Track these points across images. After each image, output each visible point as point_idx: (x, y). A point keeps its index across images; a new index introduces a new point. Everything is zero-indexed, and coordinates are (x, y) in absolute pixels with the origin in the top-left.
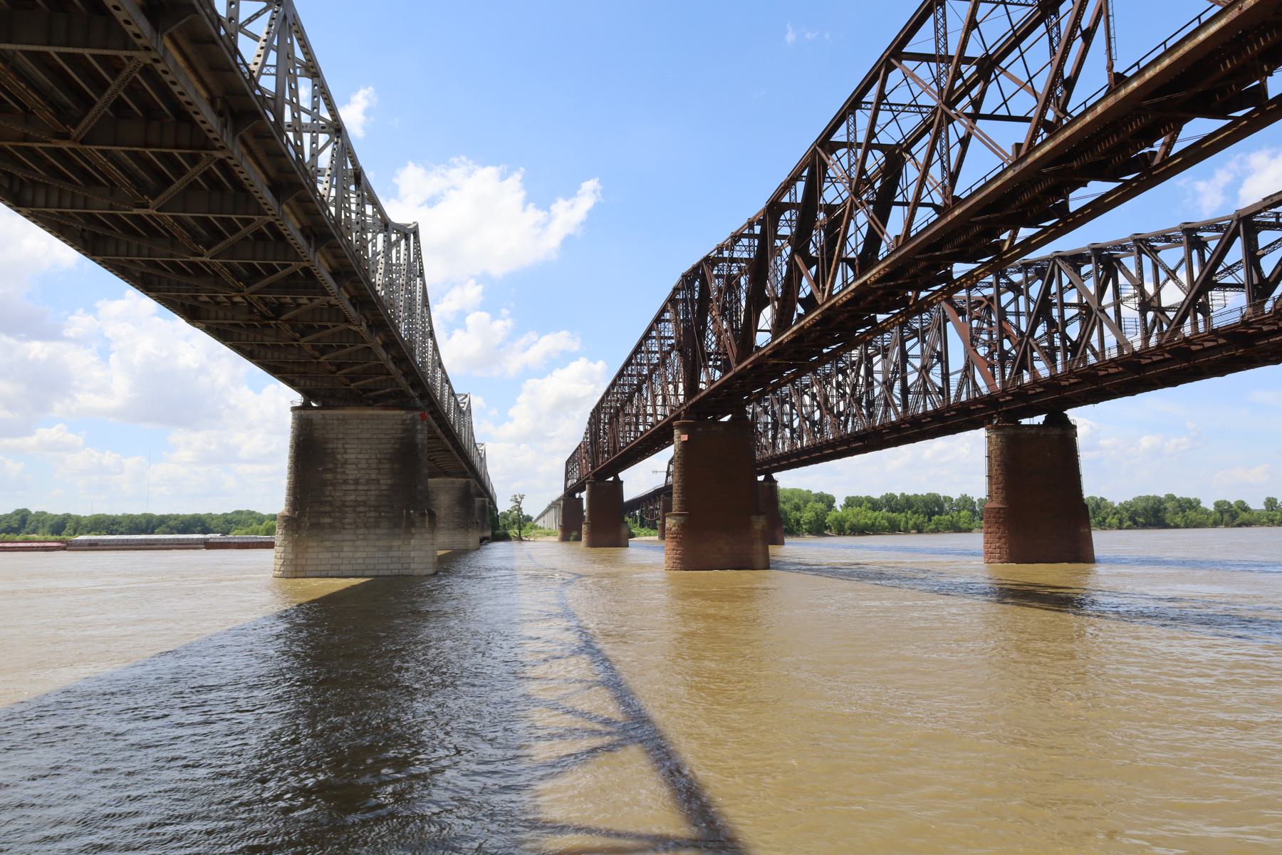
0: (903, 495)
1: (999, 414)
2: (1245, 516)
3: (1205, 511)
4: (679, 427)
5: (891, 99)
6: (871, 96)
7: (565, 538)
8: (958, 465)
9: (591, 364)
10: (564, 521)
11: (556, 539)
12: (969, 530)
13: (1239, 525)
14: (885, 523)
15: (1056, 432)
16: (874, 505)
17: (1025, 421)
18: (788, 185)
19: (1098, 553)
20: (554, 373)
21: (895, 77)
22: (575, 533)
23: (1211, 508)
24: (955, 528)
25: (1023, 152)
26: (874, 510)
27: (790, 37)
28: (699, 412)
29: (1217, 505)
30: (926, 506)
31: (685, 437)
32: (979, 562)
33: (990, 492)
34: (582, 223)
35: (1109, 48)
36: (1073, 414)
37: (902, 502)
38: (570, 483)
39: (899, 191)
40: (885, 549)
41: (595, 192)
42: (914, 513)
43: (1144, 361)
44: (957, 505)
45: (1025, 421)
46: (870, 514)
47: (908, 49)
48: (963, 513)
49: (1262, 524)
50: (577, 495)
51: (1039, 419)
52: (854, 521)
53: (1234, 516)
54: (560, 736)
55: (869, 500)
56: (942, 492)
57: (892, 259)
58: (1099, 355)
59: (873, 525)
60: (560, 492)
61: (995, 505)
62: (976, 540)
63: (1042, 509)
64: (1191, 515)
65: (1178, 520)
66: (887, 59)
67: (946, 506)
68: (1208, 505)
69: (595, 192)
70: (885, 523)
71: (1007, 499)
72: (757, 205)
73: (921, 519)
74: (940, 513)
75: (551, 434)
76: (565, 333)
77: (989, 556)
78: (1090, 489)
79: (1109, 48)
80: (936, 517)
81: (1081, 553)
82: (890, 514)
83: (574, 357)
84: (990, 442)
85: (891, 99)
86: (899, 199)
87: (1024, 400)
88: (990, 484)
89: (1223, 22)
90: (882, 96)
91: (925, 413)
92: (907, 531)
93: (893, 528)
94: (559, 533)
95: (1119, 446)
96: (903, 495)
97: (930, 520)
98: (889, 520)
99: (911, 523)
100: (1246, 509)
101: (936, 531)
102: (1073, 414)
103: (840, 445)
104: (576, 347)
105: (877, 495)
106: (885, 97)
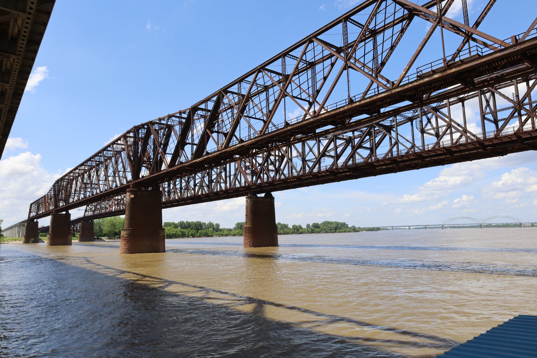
0: (187, 222)
1: (250, 192)
2: (301, 230)
3: (290, 229)
4: (129, 191)
5: (257, 82)
6: (251, 79)
7: (27, 241)
8: (233, 211)
9: (33, 156)
10: (26, 233)
11: (22, 242)
12: (212, 236)
13: (299, 234)
14: (180, 233)
15: (269, 200)
16: (176, 226)
17: (259, 195)
18: (206, 101)
19: (279, 243)
20: (10, 158)
21: (260, 75)
22: (33, 239)
23: (291, 227)
24: (207, 235)
25: (316, 114)
26: (176, 228)
27: (148, 26)
28: (137, 186)
29: (293, 226)
30: (196, 226)
31: (132, 196)
32: (242, 247)
33: (246, 221)
34: (35, 87)
35: (349, 91)
36: (274, 194)
37: (187, 225)
38: (87, 213)
39: (245, 111)
40: (176, 243)
41: (45, 73)
42: (192, 229)
43: (303, 178)
44: (208, 226)
45: (259, 195)
46: (174, 229)
47: (266, 67)
48: (210, 229)
49: (306, 233)
50: (35, 220)
51: (263, 195)
52: (168, 232)
53: (298, 230)
54: (429, 267)
55: (173, 224)
56: (202, 221)
57: (259, 139)
58: (217, 169)
59: (176, 234)
60: (26, 218)
61: (248, 226)
62: (241, 240)
63: (262, 228)
64: (286, 230)
65: (282, 232)
66: (259, 69)
67: (204, 227)
68: (304, 226)
69: (45, 73)
70: (180, 233)
71: (252, 224)
72: (188, 105)
73: (193, 231)
74: (201, 229)
75: (4, 189)
76: (20, 139)
77: (245, 245)
78: (279, 219)
79: (349, 91)
80: (200, 231)
81: (274, 243)
82: (182, 230)
83: (24, 151)
84: (247, 203)
85: (257, 82)
86: (246, 114)
87: (260, 188)
88: (247, 218)
89: (386, 94)
90: (255, 81)
91: (221, 190)
92: (188, 237)
93: (183, 235)
94: (23, 239)
95: (289, 207)
96: (187, 222)
97: (197, 232)
98: (182, 232)
99: (190, 233)
100: (301, 228)
101: (200, 236)
102: (274, 194)
103: (181, 201)
104: (25, 146)
105: (176, 222)
106: (256, 81)
